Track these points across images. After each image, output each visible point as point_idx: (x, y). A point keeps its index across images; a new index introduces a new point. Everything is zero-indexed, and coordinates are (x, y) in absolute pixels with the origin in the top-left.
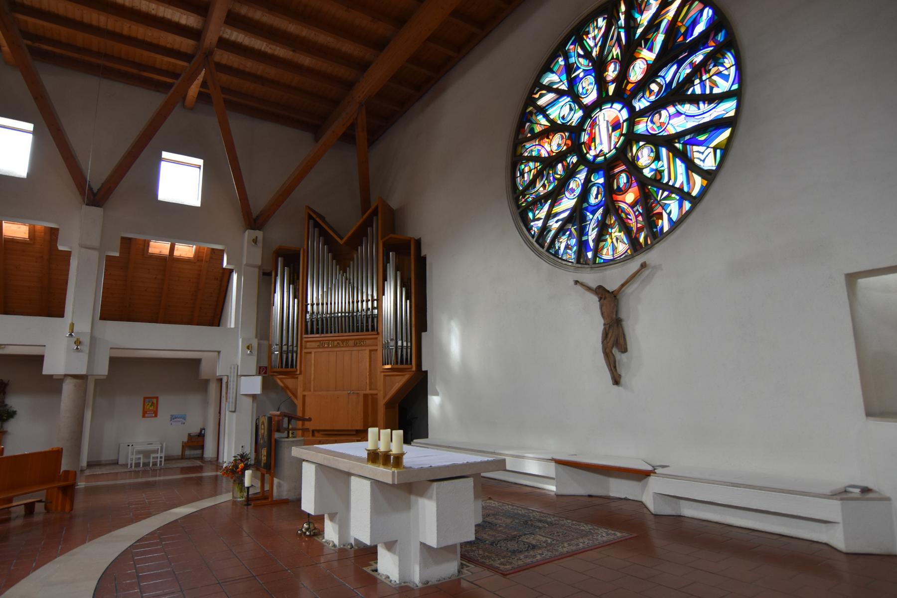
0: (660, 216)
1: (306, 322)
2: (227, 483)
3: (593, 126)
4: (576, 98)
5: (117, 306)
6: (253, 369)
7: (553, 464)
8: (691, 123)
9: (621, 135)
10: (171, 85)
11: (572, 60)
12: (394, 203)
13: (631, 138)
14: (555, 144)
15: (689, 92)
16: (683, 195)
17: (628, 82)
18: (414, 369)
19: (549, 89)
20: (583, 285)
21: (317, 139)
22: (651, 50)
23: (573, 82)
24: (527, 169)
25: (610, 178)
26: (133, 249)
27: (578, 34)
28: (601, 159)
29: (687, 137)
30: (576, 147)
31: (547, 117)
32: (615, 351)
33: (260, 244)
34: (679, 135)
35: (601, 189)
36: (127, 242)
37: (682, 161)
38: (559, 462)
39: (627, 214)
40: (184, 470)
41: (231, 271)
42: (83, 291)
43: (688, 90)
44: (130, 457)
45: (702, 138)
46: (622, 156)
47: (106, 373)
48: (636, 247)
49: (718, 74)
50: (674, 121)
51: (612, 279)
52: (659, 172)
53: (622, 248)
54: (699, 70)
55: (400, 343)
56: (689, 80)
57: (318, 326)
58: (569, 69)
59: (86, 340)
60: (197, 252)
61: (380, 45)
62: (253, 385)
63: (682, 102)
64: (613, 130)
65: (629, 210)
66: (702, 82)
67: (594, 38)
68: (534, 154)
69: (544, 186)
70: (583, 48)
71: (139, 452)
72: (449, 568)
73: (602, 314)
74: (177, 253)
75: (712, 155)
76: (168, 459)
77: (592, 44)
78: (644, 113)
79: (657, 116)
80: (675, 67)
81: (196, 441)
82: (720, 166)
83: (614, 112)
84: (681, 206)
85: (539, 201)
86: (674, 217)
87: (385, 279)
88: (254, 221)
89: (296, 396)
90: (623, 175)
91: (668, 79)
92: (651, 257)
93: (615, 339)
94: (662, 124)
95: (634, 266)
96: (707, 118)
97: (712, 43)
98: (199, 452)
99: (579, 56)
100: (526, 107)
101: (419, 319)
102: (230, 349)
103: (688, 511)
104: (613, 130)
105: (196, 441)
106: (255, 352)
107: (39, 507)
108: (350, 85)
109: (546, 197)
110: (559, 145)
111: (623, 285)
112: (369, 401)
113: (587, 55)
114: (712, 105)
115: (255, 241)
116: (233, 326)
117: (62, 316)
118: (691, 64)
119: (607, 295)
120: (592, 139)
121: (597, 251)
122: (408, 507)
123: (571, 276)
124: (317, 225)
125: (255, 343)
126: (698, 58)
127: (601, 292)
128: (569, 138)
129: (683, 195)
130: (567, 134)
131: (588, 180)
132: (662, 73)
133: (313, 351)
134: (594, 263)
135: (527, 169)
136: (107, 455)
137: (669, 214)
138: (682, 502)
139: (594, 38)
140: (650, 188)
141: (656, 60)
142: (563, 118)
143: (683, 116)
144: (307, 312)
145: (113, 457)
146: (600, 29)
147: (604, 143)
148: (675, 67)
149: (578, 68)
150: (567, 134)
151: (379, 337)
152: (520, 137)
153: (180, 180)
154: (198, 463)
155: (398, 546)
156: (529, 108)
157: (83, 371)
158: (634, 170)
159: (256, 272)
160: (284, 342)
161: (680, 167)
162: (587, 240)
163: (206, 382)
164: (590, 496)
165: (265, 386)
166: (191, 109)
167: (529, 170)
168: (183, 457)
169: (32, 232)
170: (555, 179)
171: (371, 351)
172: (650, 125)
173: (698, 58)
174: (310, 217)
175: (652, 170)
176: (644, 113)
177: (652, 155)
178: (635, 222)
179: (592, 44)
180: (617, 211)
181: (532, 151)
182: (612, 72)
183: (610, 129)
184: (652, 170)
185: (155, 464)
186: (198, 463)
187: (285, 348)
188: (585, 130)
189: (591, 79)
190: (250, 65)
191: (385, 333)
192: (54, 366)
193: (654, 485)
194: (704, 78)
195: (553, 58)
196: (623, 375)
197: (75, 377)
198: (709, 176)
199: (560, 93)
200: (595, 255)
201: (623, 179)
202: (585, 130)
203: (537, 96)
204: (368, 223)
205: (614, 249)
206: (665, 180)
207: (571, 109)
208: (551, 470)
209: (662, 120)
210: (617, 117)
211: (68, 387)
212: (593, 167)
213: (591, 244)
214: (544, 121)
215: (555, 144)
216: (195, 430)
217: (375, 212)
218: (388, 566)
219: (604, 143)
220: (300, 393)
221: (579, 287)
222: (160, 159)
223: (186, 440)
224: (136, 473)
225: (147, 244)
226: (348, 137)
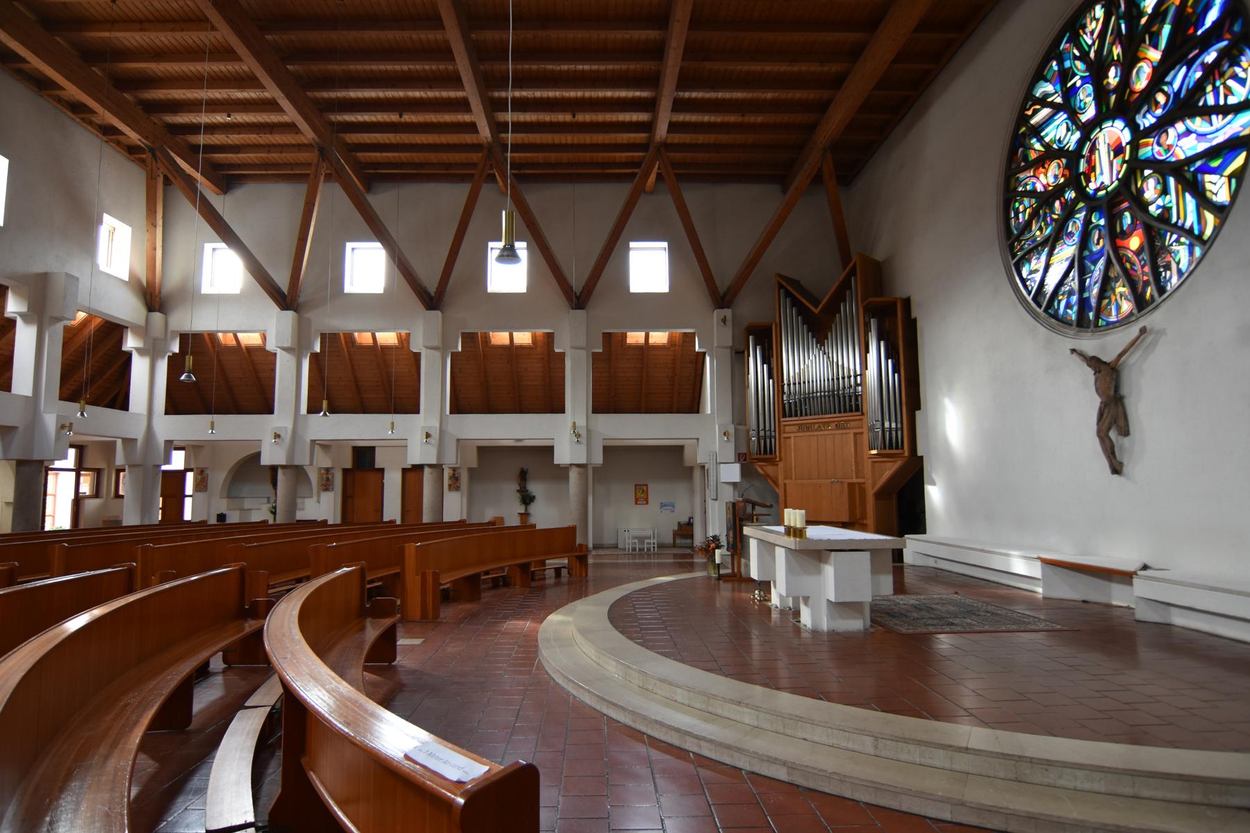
0: (1168, 267)
1: (784, 405)
2: (699, 559)
3: (1093, 149)
4: (1073, 114)
5: (607, 400)
6: (731, 455)
7: (1039, 563)
8: (1203, 146)
9: (1124, 162)
10: (634, 175)
11: (1067, 64)
12: (879, 255)
13: (1135, 167)
14: (1049, 177)
15: (1201, 104)
16: (1195, 238)
17: (1132, 92)
18: (906, 454)
19: (1043, 101)
20: (1081, 355)
21: (784, 192)
22: (1156, 47)
23: (1070, 93)
24: (1021, 209)
25: (1113, 218)
26: (613, 342)
27: (1074, 27)
28: (1102, 193)
29: (1198, 164)
30: (1075, 179)
31: (1041, 140)
32: (1113, 434)
33: (729, 323)
34: (1191, 160)
35: (1103, 232)
36: (607, 337)
37: (1193, 196)
38: (1046, 562)
39: (1132, 264)
40: (675, 556)
41: (704, 354)
42: (577, 388)
43: (1199, 100)
44: (627, 542)
45: (1215, 164)
46: (1127, 191)
47: (601, 462)
48: (1141, 303)
49: (1235, 77)
50: (1184, 141)
51: (1107, 346)
52: (1166, 210)
53: (1126, 307)
54: (1212, 72)
55: (887, 425)
56: (1199, 88)
57: (797, 406)
58: (1065, 75)
59: (583, 433)
60: (670, 338)
61: (838, 82)
62: (732, 473)
63: (1192, 116)
64: (1115, 157)
65: (1135, 259)
66: (1216, 91)
67: (1092, 33)
68: (1028, 188)
69: (1041, 229)
70: (1079, 47)
71: (635, 538)
72: (856, 624)
73: (1097, 390)
74: (651, 341)
75: (1226, 186)
76: (661, 546)
77: (1090, 42)
78: (1149, 132)
79: (1164, 135)
80: (1184, 69)
81: (685, 530)
82: (1234, 197)
83: (1116, 131)
84: (1191, 253)
85: (1036, 248)
86: (1184, 266)
87: (867, 351)
88: (721, 299)
89: (777, 485)
90: (1127, 214)
91: (1176, 86)
92: (1153, 319)
93: (1114, 416)
94: (1170, 147)
95: (1134, 330)
96: (1221, 138)
97: (1228, 36)
98: (689, 541)
99: (1076, 58)
100: (1018, 127)
101: (910, 395)
102: (708, 435)
103: (1180, 620)
104: (1115, 157)
105: (685, 530)
106: (732, 439)
107: (564, 572)
108: (812, 128)
109: (1044, 243)
110: (1056, 177)
111: (1121, 355)
112: (855, 492)
113: (1084, 57)
114: (1230, 117)
115: (724, 320)
116: (709, 412)
117: (563, 412)
118: (1203, 64)
119: (1103, 367)
120: (1092, 168)
121: (1099, 311)
122: (819, 572)
123: (1066, 342)
124: (788, 294)
125: (731, 429)
126: (1210, 57)
127: (1094, 362)
128: (1067, 167)
129: (1195, 238)
130: (1064, 161)
131: (1087, 221)
132: (1168, 79)
133: (792, 435)
134: (1096, 326)
135: (1021, 209)
136: (608, 540)
137: (1178, 263)
138: (1173, 610)
139: (1092, 33)
140: (1158, 229)
141: (1162, 61)
142: (1059, 141)
143: (1193, 136)
144: (783, 393)
145: (613, 542)
146: (1098, 20)
147: (1105, 174)
148: (1184, 69)
149: (1074, 75)
150: (1064, 161)
151: (864, 418)
152: (1013, 166)
153: (649, 267)
154: (689, 551)
155: (810, 601)
156: (1024, 129)
157: (583, 461)
158: (1140, 205)
159: (727, 353)
160: (761, 427)
161: (1191, 202)
162: (1088, 298)
163: (691, 469)
164: (1084, 602)
165: (745, 472)
166: (651, 193)
167: (1024, 207)
168: (674, 545)
169: (534, 338)
170: (1052, 219)
171: (855, 434)
172: (1157, 148)
173: (1210, 57)
174: (781, 286)
175: (1158, 207)
176: (1149, 132)
177: (1159, 187)
178: (1143, 272)
179: (1090, 42)
180: (1121, 260)
181: (1026, 184)
182: (1113, 78)
183: (1112, 154)
184: (1158, 207)
185: (649, 550)
186: (689, 551)
187: (762, 433)
188: (1083, 157)
189: (1089, 88)
190: (701, 138)
191: (870, 414)
192: (563, 456)
193: (1141, 588)
194: (1218, 83)
195: (1045, 62)
196: (1125, 463)
197: (578, 466)
198: (1221, 211)
199: (1057, 108)
200: (1097, 317)
201: (1127, 219)
202: (1083, 157)
203: (1030, 113)
204: (845, 285)
205: (1118, 308)
206: (1174, 220)
207: (1068, 130)
208: (1036, 570)
209: (1169, 142)
210: (1119, 138)
211: (573, 475)
212: (1093, 204)
213: (1093, 301)
214: (1038, 146)
215: (1049, 177)
216: (684, 519)
217: (854, 269)
218: (806, 618)
219: (1105, 174)
220: (781, 482)
221: (1075, 355)
222: (628, 249)
223: (676, 528)
224: (634, 556)
225: (624, 336)
226: (817, 179)
